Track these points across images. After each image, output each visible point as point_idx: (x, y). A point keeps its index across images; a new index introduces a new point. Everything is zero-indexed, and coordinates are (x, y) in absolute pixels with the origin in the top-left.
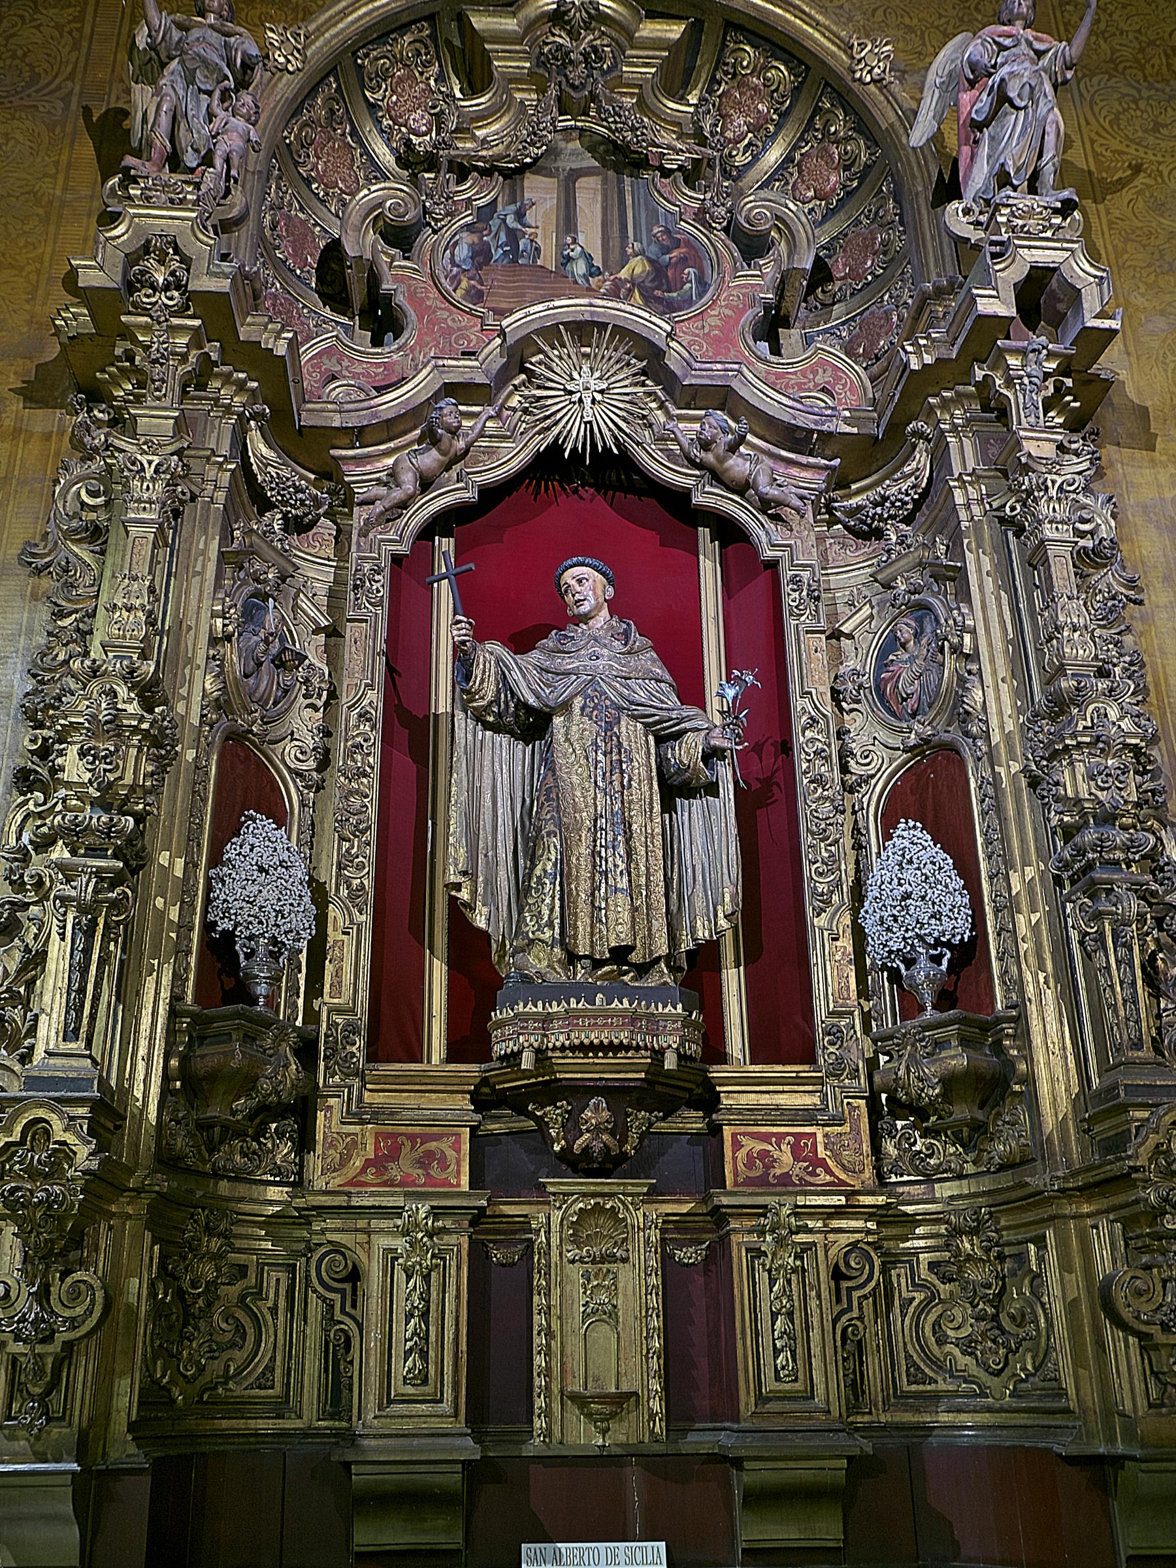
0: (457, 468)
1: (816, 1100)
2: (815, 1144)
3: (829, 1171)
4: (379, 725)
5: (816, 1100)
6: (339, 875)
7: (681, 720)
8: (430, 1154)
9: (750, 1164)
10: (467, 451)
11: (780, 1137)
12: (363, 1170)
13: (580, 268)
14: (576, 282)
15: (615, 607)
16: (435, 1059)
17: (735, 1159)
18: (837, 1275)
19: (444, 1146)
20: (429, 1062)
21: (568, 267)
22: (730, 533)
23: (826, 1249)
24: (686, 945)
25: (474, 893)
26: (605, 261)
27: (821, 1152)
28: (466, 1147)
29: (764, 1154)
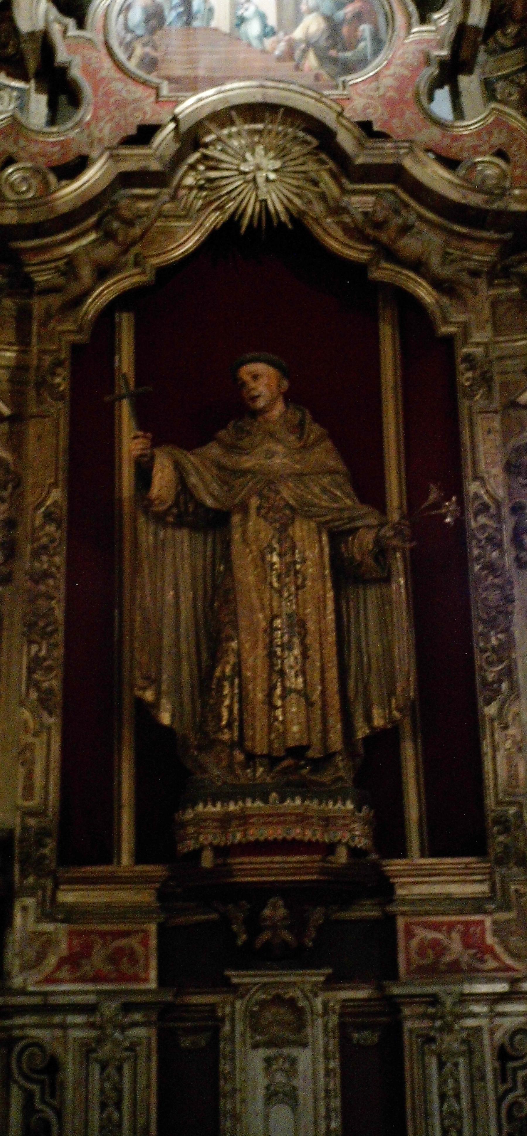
0: (135, 250)
1: (484, 888)
2: (483, 932)
3: (496, 957)
4: (64, 525)
5: (484, 888)
6: (29, 678)
7: (352, 519)
8: (120, 952)
9: (422, 953)
10: (142, 236)
11: (451, 926)
12: (59, 967)
13: (253, 29)
14: (249, 45)
15: (290, 398)
16: (126, 859)
17: (407, 948)
18: (503, 1055)
19: (134, 942)
20: (119, 863)
21: (243, 28)
22: (408, 305)
23: (492, 1032)
24: (362, 732)
25: (158, 694)
26: (280, 21)
27: (490, 940)
28: (153, 942)
29: (435, 944)
